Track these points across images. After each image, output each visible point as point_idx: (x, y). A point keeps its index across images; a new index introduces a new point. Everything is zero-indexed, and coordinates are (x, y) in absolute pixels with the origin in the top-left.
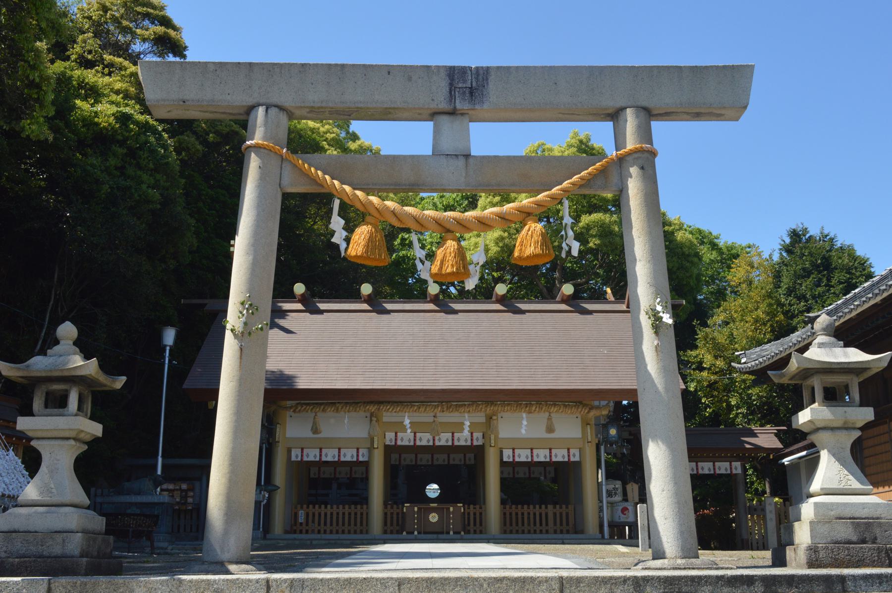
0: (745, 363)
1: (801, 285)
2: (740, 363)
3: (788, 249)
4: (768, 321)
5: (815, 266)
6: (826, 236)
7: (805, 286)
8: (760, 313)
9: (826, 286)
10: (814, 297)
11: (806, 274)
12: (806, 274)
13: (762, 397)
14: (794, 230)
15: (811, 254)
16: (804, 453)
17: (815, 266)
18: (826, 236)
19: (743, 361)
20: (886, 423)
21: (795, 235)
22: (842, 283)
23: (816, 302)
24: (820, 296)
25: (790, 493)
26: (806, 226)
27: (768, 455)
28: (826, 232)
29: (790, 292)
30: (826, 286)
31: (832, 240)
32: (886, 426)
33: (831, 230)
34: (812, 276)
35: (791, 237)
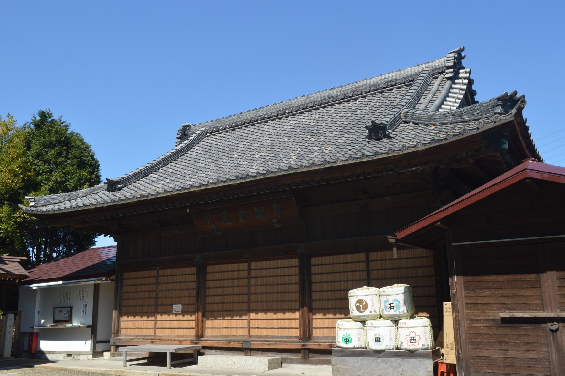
0: (33, 206)
1: (47, 152)
2: (29, 206)
3: (38, 125)
4: (21, 174)
5: (59, 142)
6: (63, 123)
7: (51, 154)
8: (14, 166)
9: (66, 157)
10: (55, 163)
11: (51, 145)
12: (51, 145)
13: (8, 232)
14: (44, 112)
15: (57, 132)
16: (60, 283)
17: (59, 142)
18: (63, 123)
19: (31, 204)
20: (155, 269)
21: (44, 116)
22: (77, 158)
23: (57, 167)
24: (61, 163)
25: (20, 308)
26: (51, 111)
27: (15, 279)
28: (63, 120)
29: (38, 155)
30: (66, 157)
31: (66, 126)
32: (155, 272)
33: (67, 119)
34: (56, 148)
35: (41, 117)
